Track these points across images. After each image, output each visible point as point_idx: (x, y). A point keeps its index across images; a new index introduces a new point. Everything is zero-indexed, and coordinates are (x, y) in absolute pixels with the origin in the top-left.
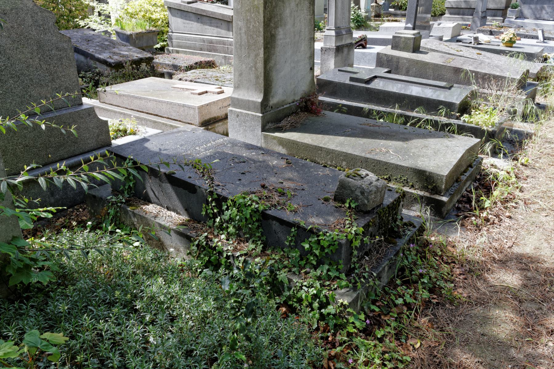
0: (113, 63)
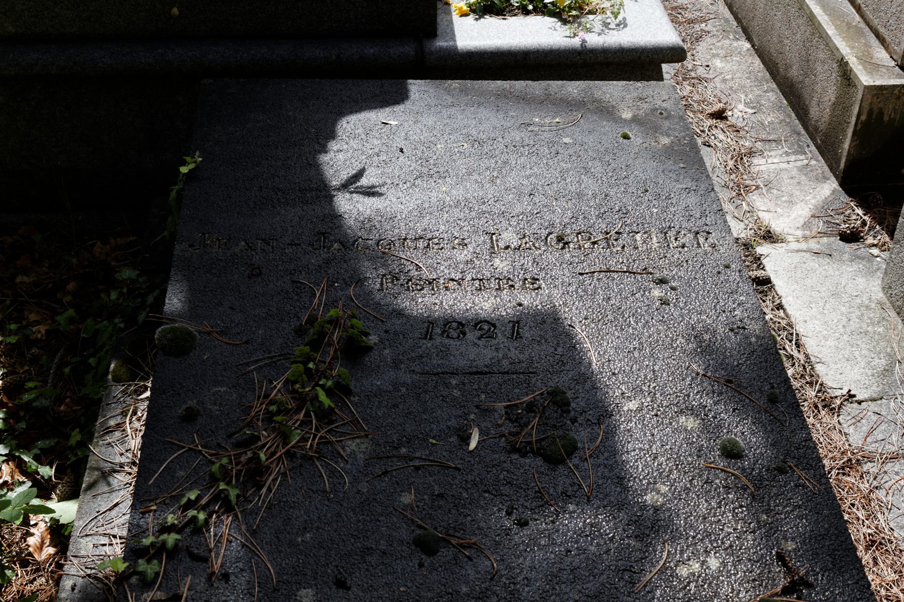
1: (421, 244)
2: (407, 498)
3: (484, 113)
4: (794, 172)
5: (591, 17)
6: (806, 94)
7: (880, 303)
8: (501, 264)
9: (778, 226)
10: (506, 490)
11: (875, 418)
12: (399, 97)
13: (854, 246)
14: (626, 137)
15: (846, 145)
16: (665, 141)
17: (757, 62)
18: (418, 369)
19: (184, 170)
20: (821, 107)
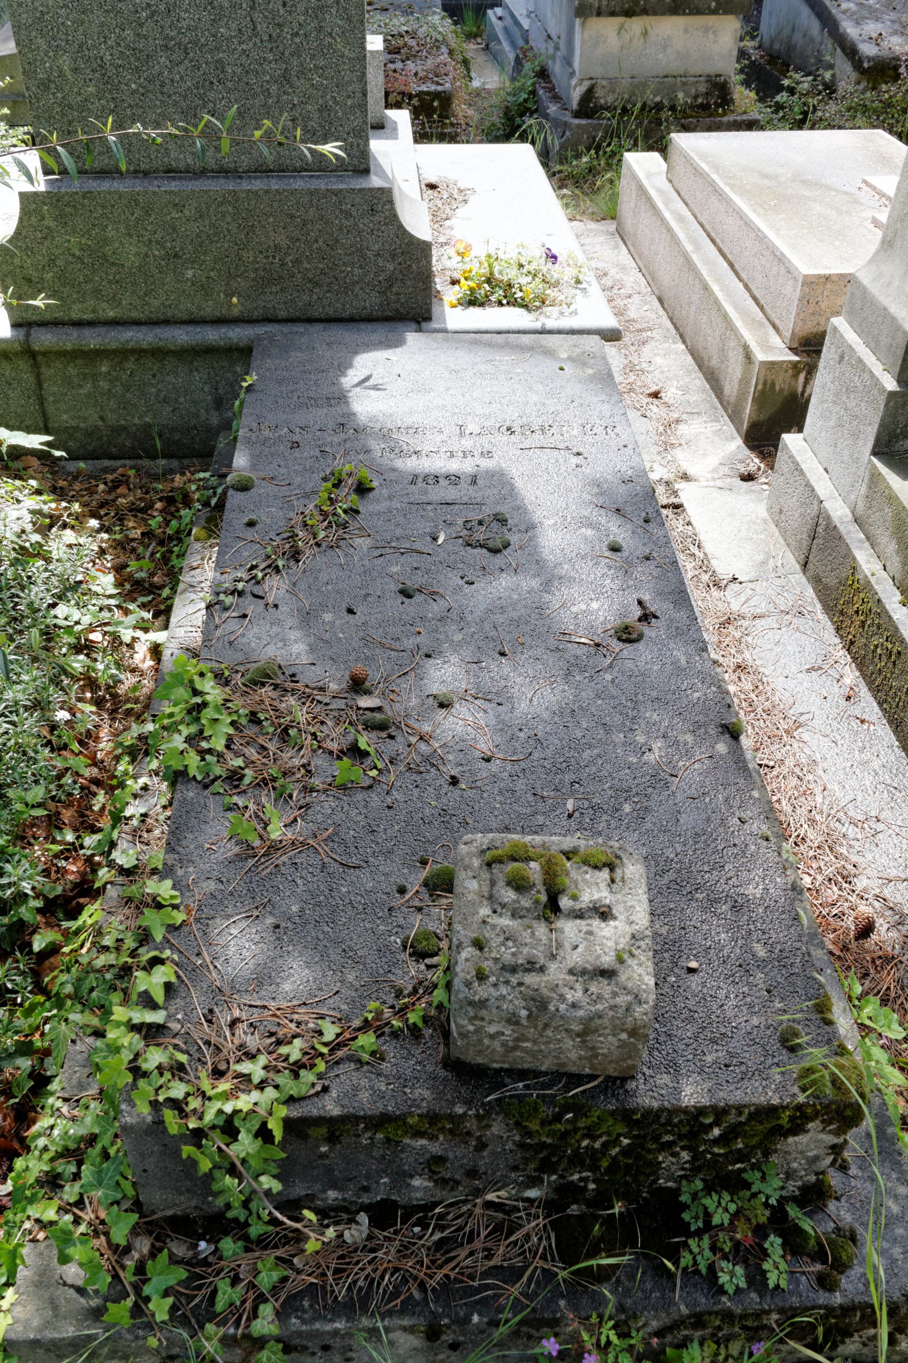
0: (869, 59)
1: (411, 431)
2: (395, 569)
3: (460, 353)
4: (710, 435)
5: (550, 308)
6: (722, 378)
7: (765, 521)
8: (467, 443)
9: (691, 472)
10: (461, 566)
11: (750, 592)
12: (399, 343)
13: (750, 483)
14: (562, 369)
15: (748, 411)
16: (591, 371)
17: (689, 358)
18: (406, 501)
19: (245, 384)
20: (731, 388)
